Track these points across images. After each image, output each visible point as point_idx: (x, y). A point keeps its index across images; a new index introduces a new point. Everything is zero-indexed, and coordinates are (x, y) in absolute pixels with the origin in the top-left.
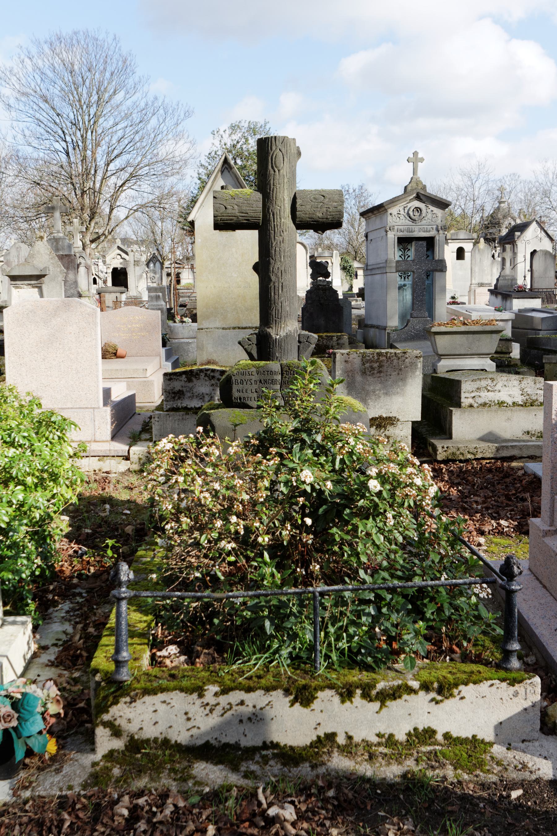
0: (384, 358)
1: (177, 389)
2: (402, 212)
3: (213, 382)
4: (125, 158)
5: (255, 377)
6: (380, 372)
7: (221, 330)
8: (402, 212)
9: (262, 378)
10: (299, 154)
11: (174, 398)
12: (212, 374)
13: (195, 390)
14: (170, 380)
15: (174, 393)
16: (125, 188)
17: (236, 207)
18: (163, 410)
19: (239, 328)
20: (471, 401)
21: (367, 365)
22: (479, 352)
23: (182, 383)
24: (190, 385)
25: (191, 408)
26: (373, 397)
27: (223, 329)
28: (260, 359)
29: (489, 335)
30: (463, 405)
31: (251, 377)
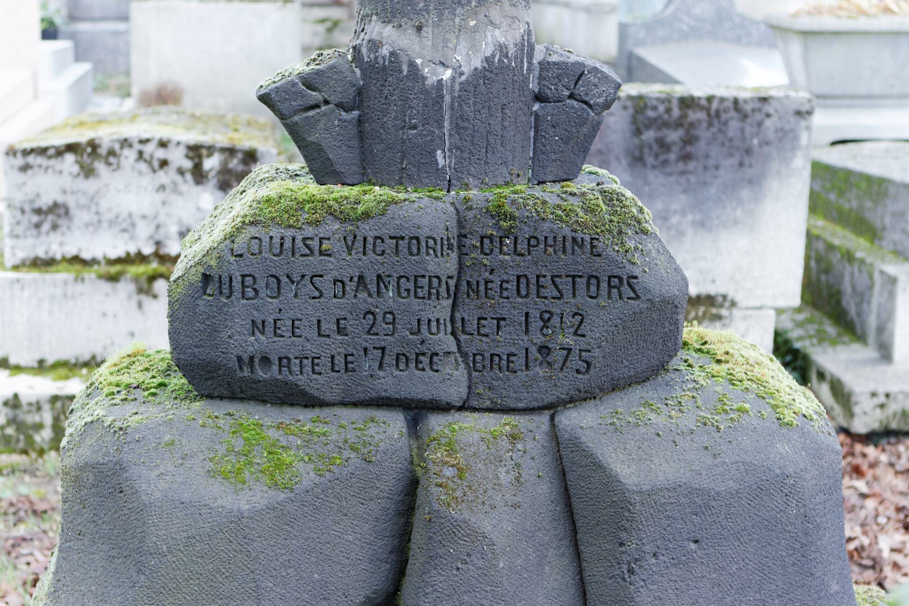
0: (701, 115)
1: (45, 201)
3: (164, 177)
5: (342, 264)
6: (686, 157)
11: (38, 226)
12: (161, 154)
13: (104, 204)
14: (25, 168)
15: (38, 211)
21: (649, 135)
23: (65, 181)
24: (90, 185)
28: (365, 177)
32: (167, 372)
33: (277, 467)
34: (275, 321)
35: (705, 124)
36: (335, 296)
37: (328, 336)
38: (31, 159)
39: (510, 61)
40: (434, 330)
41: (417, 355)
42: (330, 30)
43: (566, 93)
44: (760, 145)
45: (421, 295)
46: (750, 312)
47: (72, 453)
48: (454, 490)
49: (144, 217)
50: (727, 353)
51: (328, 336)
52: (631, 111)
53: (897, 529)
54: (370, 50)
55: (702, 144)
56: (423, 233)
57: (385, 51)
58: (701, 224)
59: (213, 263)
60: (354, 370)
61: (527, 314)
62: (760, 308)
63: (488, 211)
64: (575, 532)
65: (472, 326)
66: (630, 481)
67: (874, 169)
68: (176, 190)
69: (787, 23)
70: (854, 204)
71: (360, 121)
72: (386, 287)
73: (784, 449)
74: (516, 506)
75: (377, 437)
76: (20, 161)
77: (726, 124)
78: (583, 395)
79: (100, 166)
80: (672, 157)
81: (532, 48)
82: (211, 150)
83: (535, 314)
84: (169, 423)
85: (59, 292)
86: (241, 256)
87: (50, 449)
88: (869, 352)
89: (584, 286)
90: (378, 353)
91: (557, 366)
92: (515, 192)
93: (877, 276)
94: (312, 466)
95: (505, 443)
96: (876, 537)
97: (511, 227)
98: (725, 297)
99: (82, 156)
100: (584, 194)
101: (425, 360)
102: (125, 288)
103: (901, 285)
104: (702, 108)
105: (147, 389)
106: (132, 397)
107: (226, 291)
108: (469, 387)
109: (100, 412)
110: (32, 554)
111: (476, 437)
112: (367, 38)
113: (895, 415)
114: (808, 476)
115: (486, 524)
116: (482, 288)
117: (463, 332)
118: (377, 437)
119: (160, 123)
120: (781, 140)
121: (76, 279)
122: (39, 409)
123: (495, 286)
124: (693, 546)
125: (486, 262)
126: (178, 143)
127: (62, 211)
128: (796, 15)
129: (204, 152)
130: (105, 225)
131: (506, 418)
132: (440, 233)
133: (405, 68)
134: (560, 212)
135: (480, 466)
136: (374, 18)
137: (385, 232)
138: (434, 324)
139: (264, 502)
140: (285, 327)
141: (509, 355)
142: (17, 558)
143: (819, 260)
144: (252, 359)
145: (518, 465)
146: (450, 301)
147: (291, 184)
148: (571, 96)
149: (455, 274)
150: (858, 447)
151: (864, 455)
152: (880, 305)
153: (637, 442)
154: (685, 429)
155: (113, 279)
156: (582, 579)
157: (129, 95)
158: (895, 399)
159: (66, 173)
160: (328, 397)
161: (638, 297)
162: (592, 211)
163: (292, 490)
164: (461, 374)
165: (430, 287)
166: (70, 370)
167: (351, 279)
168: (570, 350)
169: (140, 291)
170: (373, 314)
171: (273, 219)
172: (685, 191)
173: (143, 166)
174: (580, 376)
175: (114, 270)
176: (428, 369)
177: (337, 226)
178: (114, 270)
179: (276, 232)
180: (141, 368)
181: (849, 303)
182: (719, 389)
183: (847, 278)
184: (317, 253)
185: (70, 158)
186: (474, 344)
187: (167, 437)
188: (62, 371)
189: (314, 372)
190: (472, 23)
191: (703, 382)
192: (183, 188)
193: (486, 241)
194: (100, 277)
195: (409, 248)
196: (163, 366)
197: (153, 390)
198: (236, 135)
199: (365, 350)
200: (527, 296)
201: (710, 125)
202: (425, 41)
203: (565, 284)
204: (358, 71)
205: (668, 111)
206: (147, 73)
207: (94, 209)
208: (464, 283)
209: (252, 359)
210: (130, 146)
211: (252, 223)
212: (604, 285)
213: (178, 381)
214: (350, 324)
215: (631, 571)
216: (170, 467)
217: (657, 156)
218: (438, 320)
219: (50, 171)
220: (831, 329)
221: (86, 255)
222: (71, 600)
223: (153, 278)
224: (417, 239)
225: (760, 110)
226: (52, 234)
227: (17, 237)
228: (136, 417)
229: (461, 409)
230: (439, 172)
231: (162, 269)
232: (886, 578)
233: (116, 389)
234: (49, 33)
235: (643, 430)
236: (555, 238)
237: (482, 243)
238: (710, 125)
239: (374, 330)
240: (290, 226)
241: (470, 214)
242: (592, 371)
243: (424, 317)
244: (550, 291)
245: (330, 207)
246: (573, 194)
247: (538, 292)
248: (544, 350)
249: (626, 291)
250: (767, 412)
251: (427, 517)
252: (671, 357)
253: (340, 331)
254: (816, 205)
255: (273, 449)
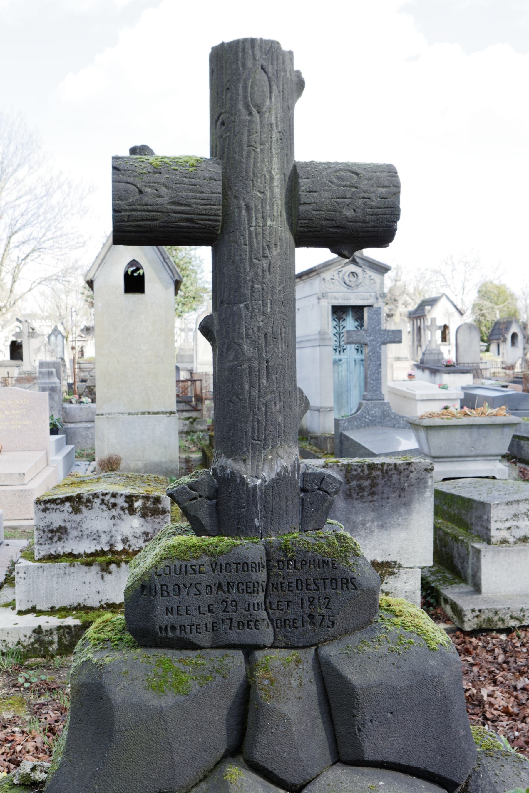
0: (379, 473)
1: (56, 525)
2: (336, 277)
3: (114, 512)
4: (27, 231)
5: (209, 577)
6: (373, 494)
7: (126, 416)
8: (336, 277)
9: (224, 577)
10: (300, 85)
11: (51, 539)
12: (113, 500)
13: (84, 526)
14: (45, 510)
15: (52, 531)
16: (27, 261)
17: (163, 190)
18: (32, 559)
19: (149, 413)
20: (505, 534)
21: (354, 483)
22: (487, 452)
23: (65, 516)
24: (78, 517)
25: (80, 555)
26: (363, 533)
27: (129, 414)
28: (219, 530)
29: (499, 430)
30: (493, 540)
31: (198, 577)
32: (122, 632)
33: (180, 683)
34: (178, 607)
35: (381, 477)
36: (207, 594)
37: (204, 614)
38: (48, 505)
39: (289, 474)
40: (256, 608)
41: (248, 621)
42: (192, 423)
43: (316, 487)
44: (409, 486)
45: (249, 591)
46: (408, 570)
47: (76, 677)
48: (269, 692)
49: (104, 532)
50: (401, 611)
51: (204, 614)
52: (344, 472)
53: (490, 683)
54: (221, 470)
55: (380, 487)
56: (250, 561)
57: (228, 471)
58: (382, 527)
59: (146, 579)
60: (217, 630)
61: (302, 599)
62: (413, 567)
63: (281, 548)
64: (330, 710)
65: (275, 606)
66: (356, 683)
67: (465, 494)
68: (120, 518)
69: (417, 422)
70: (456, 511)
71: (217, 505)
72: (232, 588)
73: (433, 662)
74: (300, 698)
75: (229, 665)
76: (43, 507)
77: (391, 476)
78: (331, 638)
79: (83, 508)
80: (366, 494)
81: (299, 466)
82: (137, 497)
83: (306, 598)
84: (125, 662)
85: (62, 572)
86: (160, 575)
87: (57, 655)
88: (469, 588)
89: (329, 584)
90: (229, 621)
91: (318, 624)
92: (294, 538)
93: (470, 549)
94: (197, 682)
95: (293, 665)
96: (480, 689)
97: (292, 556)
98: (395, 562)
99: (74, 503)
100: (327, 537)
101: (252, 624)
102: (95, 569)
103: (483, 554)
104: (379, 469)
105: (113, 642)
106: (106, 647)
107: (154, 593)
108: (274, 637)
109: (90, 656)
110: (48, 713)
111: (279, 662)
112: (219, 465)
113: (484, 620)
114: (445, 676)
115: (286, 709)
116: (279, 586)
117: (271, 609)
118: (229, 665)
119: (111, 483)
120: (418, 484)
121: (70, 566)
122: (51, 633)
123: (286, 585)
124: (389, 715)
125: (280, 573)
126: (122, 495)
127: (64, 530)
128: (421, 418)
129: (134, 499)
130: (85, 537)
131: (293, 652)
132: (258, 560)
133: (238, 480)
134: (316, 547)
135: (281, 678)
136: (223, 455)
137: (230, 561)
138: (256, 606)
139: (174, 702)
140: (183, 611)
141: (293, 620)
142: (40, 715)
143: (441, 540)
144: (166, 627)
145: (300, 676)
146: (264, 594)
147: (183, 537)
148: (319, 489)
149: (265, 579)
150: (467, 638)
151: (471, 643)
152: (472, 563)
153: (361, 663)
154: (382, 654)
155: (89, 564)
156: (335, 735)
157: (94, 460)
158: (484, 612)
159: (66, 511)
160: (205, 644)
161: (356, 589)
162: (332, 546)
163: (187, 695)
164: (270, 630)
165: (254, 587)
166: (67, 612)
167: (215, 585)
168: (323, 616)
169: (103, 570)
170: (226, 602)
171: (176, 556)
172: (373, 511)
173: (104, 507)
174: (329, 629)
175: (89, 560)
176: (253, 628)
177: (207, 559)
178: (89, 560)
179: (176, 563)
180: (109, 629)
181: (458, 562)
182: (398, 632)
183: (455, 549)
184: (198, 572)
185: (68, 504)
186: (278, 614)
187: (124, 669)
188: (63, 613)
189: (197, 632)
190: (270, 457)
191: (390, 629)
192: (124, 517)
193: (281, 563)
194: (82, 564)
195: (243, 569)
196: (120, 628)
197: (116, 642)
198: (149, 488)
199: (223, 620)
200: (301, 590)
201: (383, 477)
202: (248, 466)
203: (320, 583)
204: (215, 481)
205: (363, 471)
206: (102, 453)
207: (79, 529)
208: (270, 584)
209: (166, 627)
210: (98, 497)
211: (165, 559)
212: (339, 583)
213: (128, 637)
214: (214, 608)
215: (359, 730)
216: (126, 685)
217: (358, 494)
218: (258, 604)
219: (58, 510)
220: (449, 576)
221: (75, 552)
222: (76, 756)
223: (109, 563)
224: (247, 564)
225: (407, 469)
226: (58, 543)
227: (41, 544)
228: (108, 659)
229: (270, 648)
230: (257, 529)
231: (114, 558)
232: (486, 711)
233: (97, 642)
234: (54, 431)
235: (362, 656)
236: (314, 560)
237: (278, 564)
238: (383, 477)
239: (227, 610)
240: (184, 560)
241: (272, 549)
242: (335, 626)
243: (251, 602)
244: (312, 586)
245: (204, 549)
246: (321, 538)
247: (307, 587)
248: (311, 616)
249: (351, 586)
250: (422, 643)
251: (256, 707)
252: (373, 616)
253: (210, 611)
254: (438, 512)
255: (177, 673)
